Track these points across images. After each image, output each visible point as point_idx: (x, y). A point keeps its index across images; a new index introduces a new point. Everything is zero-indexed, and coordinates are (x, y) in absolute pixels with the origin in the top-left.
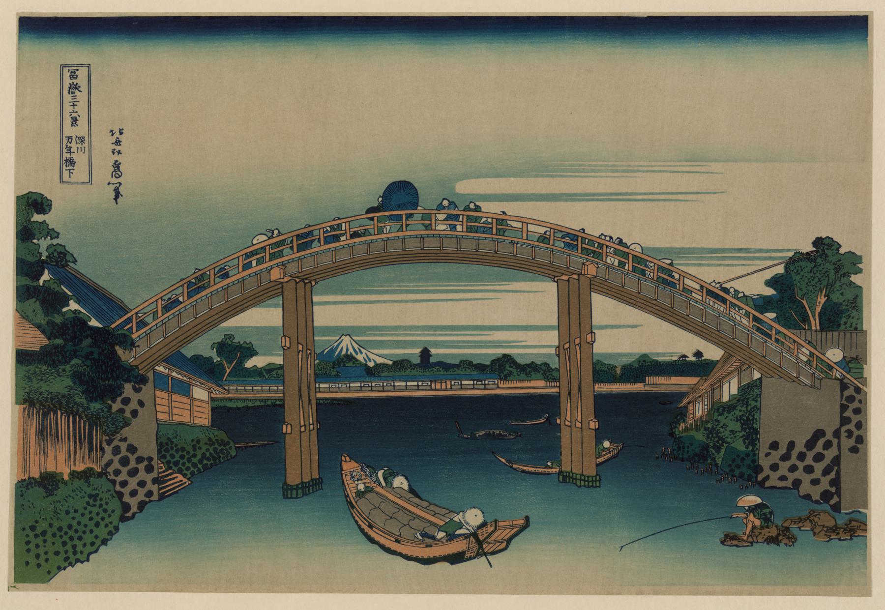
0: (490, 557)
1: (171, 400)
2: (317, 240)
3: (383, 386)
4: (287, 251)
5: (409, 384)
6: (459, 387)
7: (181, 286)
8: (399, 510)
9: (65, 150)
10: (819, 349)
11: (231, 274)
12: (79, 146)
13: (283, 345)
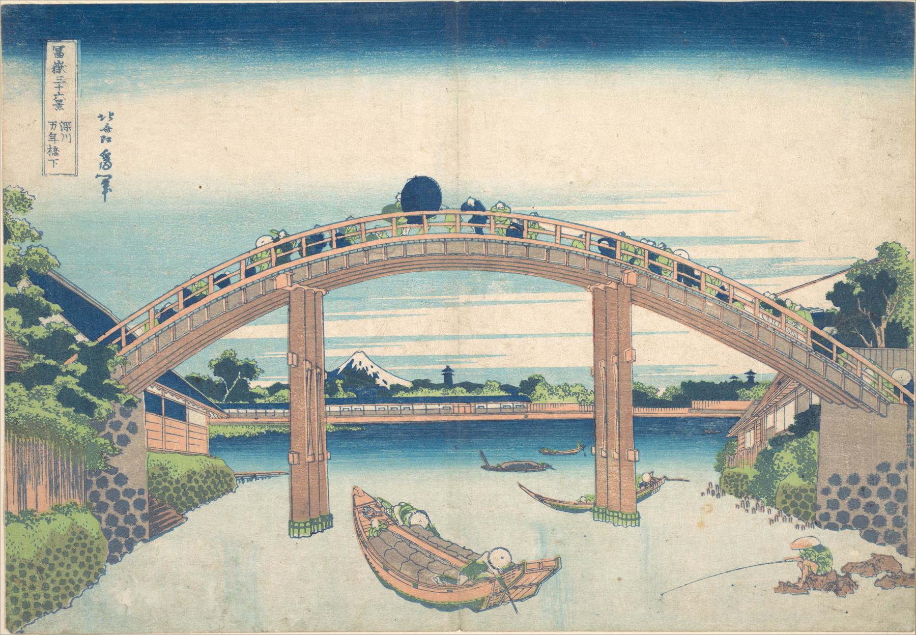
0: (517, 604)
1: (164, 426)
2: (328, 243)
3: (401, 410)
4: (295, 255)
5: (258, 411)
6: (411, 412)
7: (176, 294)
8: (417, 551)
9: (48, 138)
10: (885, 369)
11: (232, 280)
12: (64, 132)
13: (290, 363)
